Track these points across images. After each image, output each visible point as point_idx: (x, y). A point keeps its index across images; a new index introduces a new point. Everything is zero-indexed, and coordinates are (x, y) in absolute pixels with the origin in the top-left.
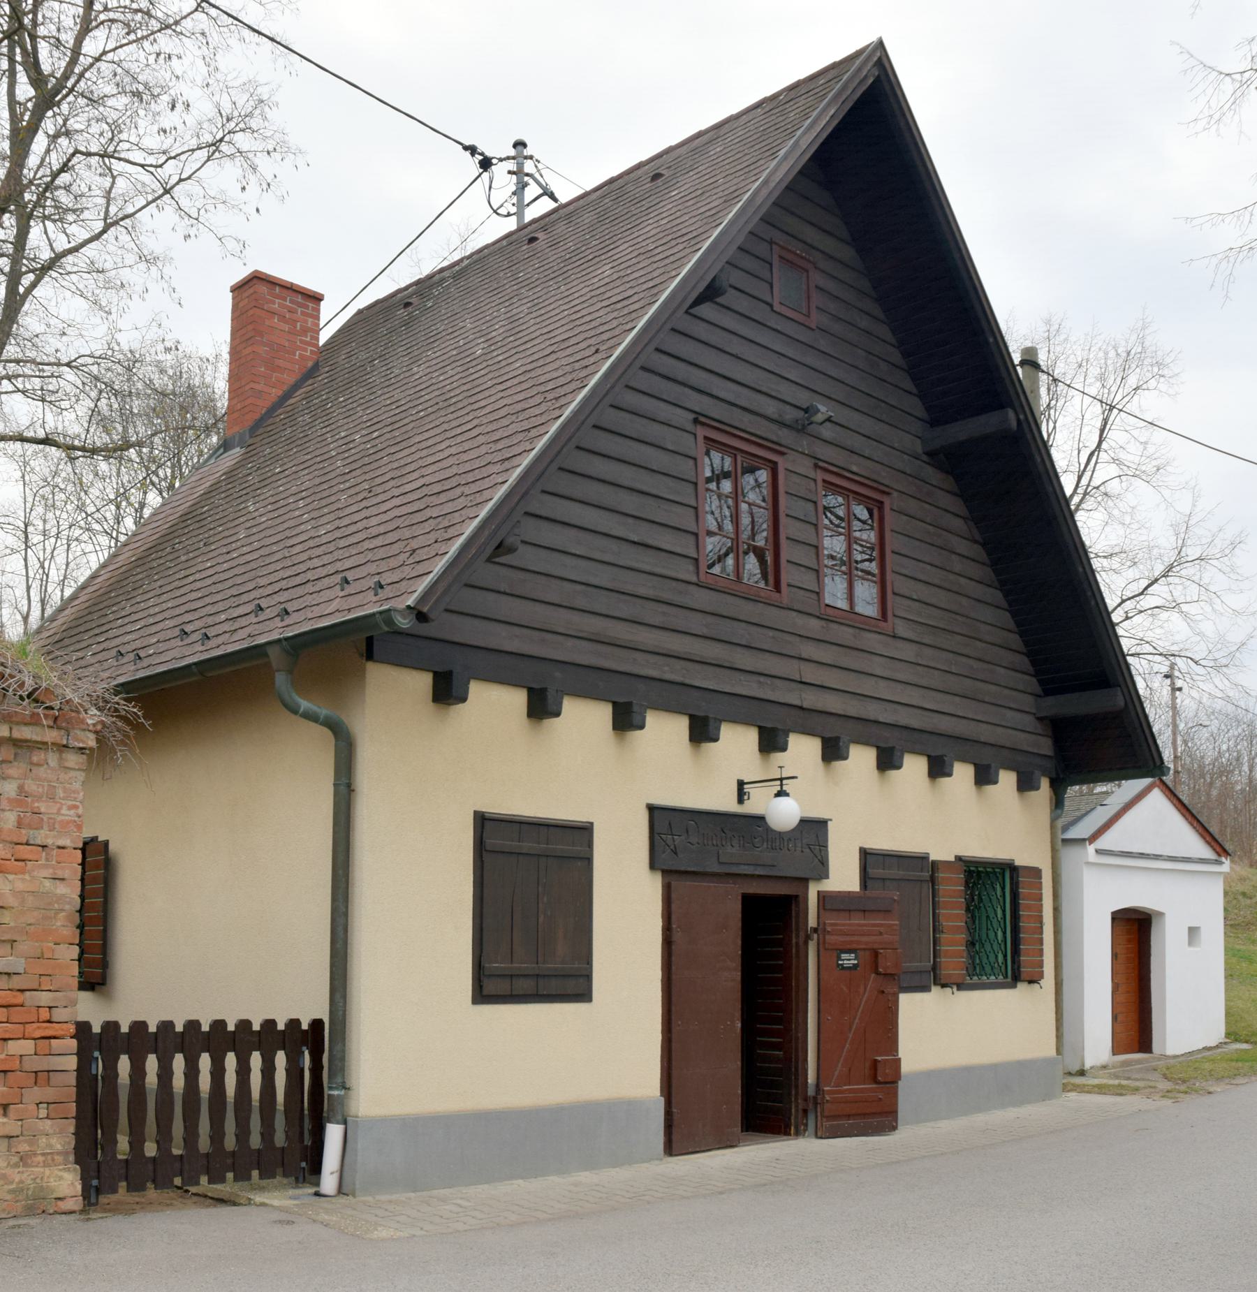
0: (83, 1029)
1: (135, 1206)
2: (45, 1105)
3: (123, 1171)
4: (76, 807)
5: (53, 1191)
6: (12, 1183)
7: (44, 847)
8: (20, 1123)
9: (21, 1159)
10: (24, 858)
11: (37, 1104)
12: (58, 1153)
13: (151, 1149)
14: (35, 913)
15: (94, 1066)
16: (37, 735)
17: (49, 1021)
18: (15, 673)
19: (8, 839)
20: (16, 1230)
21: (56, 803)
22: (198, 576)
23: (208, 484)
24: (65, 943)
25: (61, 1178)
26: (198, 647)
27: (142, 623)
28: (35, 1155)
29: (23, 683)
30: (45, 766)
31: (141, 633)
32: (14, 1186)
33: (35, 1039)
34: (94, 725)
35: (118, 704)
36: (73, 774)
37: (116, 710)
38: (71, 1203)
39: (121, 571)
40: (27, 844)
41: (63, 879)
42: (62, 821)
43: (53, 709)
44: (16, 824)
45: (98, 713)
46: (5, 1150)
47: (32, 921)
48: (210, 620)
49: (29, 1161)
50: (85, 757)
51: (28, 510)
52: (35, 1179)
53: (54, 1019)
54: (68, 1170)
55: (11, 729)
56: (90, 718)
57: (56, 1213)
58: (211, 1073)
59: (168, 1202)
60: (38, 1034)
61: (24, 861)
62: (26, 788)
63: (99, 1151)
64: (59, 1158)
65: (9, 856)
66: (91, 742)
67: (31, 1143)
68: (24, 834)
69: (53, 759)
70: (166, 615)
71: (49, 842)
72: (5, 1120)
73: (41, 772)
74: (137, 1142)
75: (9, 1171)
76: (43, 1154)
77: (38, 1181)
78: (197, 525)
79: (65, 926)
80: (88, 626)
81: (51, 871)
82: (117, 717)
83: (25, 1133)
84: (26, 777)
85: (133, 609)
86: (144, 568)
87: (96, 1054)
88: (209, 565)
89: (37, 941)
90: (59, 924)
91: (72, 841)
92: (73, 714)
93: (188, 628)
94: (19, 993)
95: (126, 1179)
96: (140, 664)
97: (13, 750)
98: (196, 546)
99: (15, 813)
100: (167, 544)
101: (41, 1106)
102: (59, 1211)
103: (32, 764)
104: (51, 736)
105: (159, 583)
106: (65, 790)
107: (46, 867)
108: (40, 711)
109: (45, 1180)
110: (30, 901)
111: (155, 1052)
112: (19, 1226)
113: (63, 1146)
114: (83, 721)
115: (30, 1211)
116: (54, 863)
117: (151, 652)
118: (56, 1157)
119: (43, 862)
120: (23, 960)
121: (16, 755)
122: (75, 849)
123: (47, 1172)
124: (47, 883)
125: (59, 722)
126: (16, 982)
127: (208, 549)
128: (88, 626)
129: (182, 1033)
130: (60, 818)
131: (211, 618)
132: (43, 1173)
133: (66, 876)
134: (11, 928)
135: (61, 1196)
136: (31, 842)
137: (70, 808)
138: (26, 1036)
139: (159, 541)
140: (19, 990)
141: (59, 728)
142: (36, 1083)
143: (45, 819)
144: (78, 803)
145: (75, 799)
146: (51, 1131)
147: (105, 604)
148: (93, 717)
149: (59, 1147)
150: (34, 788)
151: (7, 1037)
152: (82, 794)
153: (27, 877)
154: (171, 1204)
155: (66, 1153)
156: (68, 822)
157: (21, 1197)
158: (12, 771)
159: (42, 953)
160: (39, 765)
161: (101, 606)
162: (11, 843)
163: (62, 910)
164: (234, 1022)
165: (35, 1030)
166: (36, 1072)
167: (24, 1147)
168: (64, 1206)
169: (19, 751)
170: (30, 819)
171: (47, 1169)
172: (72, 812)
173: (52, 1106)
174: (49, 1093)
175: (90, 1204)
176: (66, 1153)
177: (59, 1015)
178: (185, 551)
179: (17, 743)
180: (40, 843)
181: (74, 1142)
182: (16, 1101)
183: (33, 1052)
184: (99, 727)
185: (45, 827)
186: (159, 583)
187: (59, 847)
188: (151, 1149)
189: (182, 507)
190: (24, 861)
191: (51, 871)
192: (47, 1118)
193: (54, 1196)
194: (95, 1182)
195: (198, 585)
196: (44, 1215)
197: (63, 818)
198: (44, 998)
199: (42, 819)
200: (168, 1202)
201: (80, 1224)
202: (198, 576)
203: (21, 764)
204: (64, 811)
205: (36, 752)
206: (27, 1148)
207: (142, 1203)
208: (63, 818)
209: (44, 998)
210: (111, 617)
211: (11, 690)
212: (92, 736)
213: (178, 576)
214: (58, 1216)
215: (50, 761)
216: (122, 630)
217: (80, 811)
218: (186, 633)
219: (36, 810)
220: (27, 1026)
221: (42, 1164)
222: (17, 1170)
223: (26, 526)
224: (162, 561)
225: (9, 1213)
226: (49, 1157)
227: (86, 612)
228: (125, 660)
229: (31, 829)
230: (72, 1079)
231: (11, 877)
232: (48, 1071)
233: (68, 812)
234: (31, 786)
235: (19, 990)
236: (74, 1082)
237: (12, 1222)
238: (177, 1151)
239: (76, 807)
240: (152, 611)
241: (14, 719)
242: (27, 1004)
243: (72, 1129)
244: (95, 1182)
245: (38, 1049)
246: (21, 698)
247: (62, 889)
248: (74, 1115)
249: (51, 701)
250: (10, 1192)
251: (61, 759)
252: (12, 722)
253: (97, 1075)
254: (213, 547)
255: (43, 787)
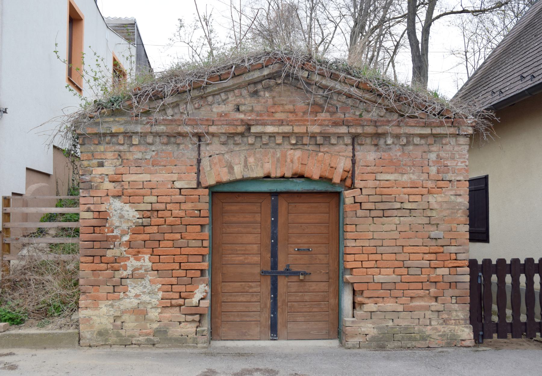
0: (472, 263)
1: (503, 344)
2: (455, 297)
3: (495, 328)
4: (465, 162)
5: (460, 336)
6: (440, 332)
7: (450, 181)
8: (443, 305)
9: (444, 321)
10: (441, 186)
11: (451, 297)
12: (462, 319)
13: (523, 318)
14: (447, 211)
15: (479, 280)
16: (444, 131)
17: (456, 260)
18: (431, 104)
19: (433, 179)
20: (441, 354)
21: (455, 161)
22: (531, 51)
23: (539, 9)
24: (462, 224)
25: (463, 331)
26: (530, 82)
27: (504, 77)
28: (451, 320)
29: (435, 108)
30: (449, 145)
31: (504, 81)
32: (441, 333)
33: (449, 268)
34: (471, 123)
35: (483, 112)
36: (463, 147)
37: (483, 115)
38: (469, 342)
39: (496, 58)
40: (443, 180)
41: (460, 195)
42: (459, 168)
43: (451, 118)
44: (436, 172)
45: (473, 118)
46: (437, 317)
47: (446, 215)
48: (535, 69)
49: (448, 322)
50: (468, 138)
51: (466, 47)
52: (451, 331)
53: (458, 259)
54: (467, 327)
55: (431, 129)
56: (469, 120)
57: (461, 346)
58: (540, 283)
59: (521, 343)
60: (450, 265)
61: (441, 188)
62: (441, 155)
63: (483, 320)
64: (462, 322)
65: (434, 186)
66: (470, 131)
67: (448, 315)
68: (440, 176)
69: (453, 141)
70: (515, 71)
71: (453, 178)
72: (436, 304)
73: (447, 147)
74: (502, 314)
75: (439, 327)
76: (454, 320)
77: (452, 331)
78: (532, 29)
79: (462, 216)
80: (481, 84)
81: (454, 192)
82: (484, 118)
83: (445, 310)
84: (439, 150)
85: (501, 72)
86: (506, 54)
87: (480, 274)
88: (536, 44)
89: (449, 224)
90: (459, 215)
91: (464, 177)
92: (461, 120)
93: (524, 75)
94: (441, 247)
95: (497, 332)
96: (502, 95)
97: (433, 139)
98: (531, 38)
99: (436, 167)
100: (517, 41)
101: (453, 298)
102: (463, 345)
103: (442, 144)
104: (452, 130)
105: (512, 59)
106: (459, 155)
107: (451, 190)
108: (444, 120)
109: (456, 331)
110: (445, 206)
111: (510, 273)
112: (443, 352)
113: (464, 316)
114: (464, 122)
115: (449, 345)
116: (455, 188)
117: (507, 89)
118: (461, 321)
119: (450, 188)
120: (442, 233)
121: (435, 141)
122: (465, 181)
123: (457, 327)
124: (453, 197)
125: (454, 124)
126: (440, 242)
127: (537, 37)
128: (481, 84)
129: (524, 264)
130: (458, 167)
131: (536, 68)
132: (455, 328)
133: (461, 194)
134: (436, 218)
135: (463, 339)
136: (444, 179)
137: (462, 162)
138: (445, 266)
139: (514, 40)
140: (441, 246)
141: (454, 127)
142: (450, 287)
143: (450, 169)
144: (466, 160)
145: (464, 158)
146: (458, 309)
147: (489, 73)
148: (471, 120)
149: (462, 317)
150: (444, 155)
151: (436, 267)
152: (467, 155)
153: (443, 195)
154: (523, 345)
155: (465, 320)
156: (462, 169)
157: (444, 339)
158: (434, 148)
159: (451, 229)
160: (446, 144)
161: (487, 74)
162: (435, 180)
163: (461, 209)
164: (524, 259)
165: (449, 264)
166: (450, 283)
167: (445, 316)
168: (464, 343)
169: (436, 139)
170: (444, 168)
171: (456, 326)
172: (463, 164)
173: (458, 298)
174: (456, 292)
175: (479, 343)
176: (465, 320)
177: (460, 256)
178: (525, 41)
179: (434, 135)
180: (448, 179)
181: (469, 315)
182: (441, 295)
183: (448, 274)
184: (474, 124)
185: (451, 172)
186: (512, 59)
187: (458, 181)
188: (523, 318)
189: (525, 23)
190: (441, 188)
191: (454, 192)
192: (456, 303)
193: (460, 338)
194: (481, 333)
195: (531, 55)
196: (455, 347)
197: (459, 167)
198: (453, 249)
199: (449, 169)
200: (521, 343)
201: (472, 353)
202: (531, 51)
203: (438, 145)
204: (459, 164)
205: (444, 139)
206: (447, 317)
207: (508, 343)
208: (459, 167)
209: (453, 249)
210: (491, 78)
211: (429, 112)
212: (470, 128)
213: (521, 53)
214: (462, 348)
215: (451, 142)
216: (495, 83)
217: (467, 163)
218: (524, 77)
219: (446, 165)
220: (445, 262)
221: (454, 324)
222: (442, 326)
223: (466, 53)
224: (514, 49)
225: (439, 345)
226: (457, 321)
227: (481, 78)
228: (496, 95)
229: (444, 173)
230: (467, 286)
231: (435, 196)
232: (456, 282)
233: (461, 165)
234: (443, 154)
235: (441, 246)
236: (468, 287)
237: (440, 350)
238: (537, 320)
239: (465, 162)
240: (508, 71)
241: (433, 125)
242: (445, 252)
243: (468, 309)
244: (481, 333)
245: (451, 272)
246: (434, 115)
247: (459, 200)
248: (469, 302)
249: (449, 114)
250: (439, 336)
251: (456, 140)
252: (431, 126)
253: (481, 284)
254: (539, 36)
255: (449, 154)
